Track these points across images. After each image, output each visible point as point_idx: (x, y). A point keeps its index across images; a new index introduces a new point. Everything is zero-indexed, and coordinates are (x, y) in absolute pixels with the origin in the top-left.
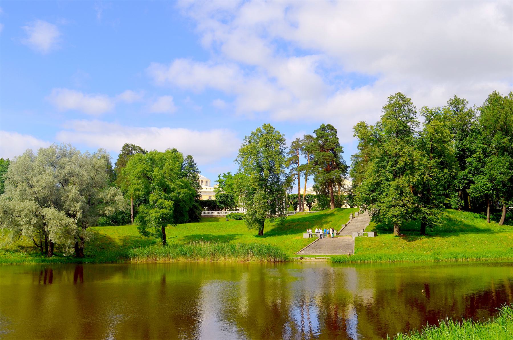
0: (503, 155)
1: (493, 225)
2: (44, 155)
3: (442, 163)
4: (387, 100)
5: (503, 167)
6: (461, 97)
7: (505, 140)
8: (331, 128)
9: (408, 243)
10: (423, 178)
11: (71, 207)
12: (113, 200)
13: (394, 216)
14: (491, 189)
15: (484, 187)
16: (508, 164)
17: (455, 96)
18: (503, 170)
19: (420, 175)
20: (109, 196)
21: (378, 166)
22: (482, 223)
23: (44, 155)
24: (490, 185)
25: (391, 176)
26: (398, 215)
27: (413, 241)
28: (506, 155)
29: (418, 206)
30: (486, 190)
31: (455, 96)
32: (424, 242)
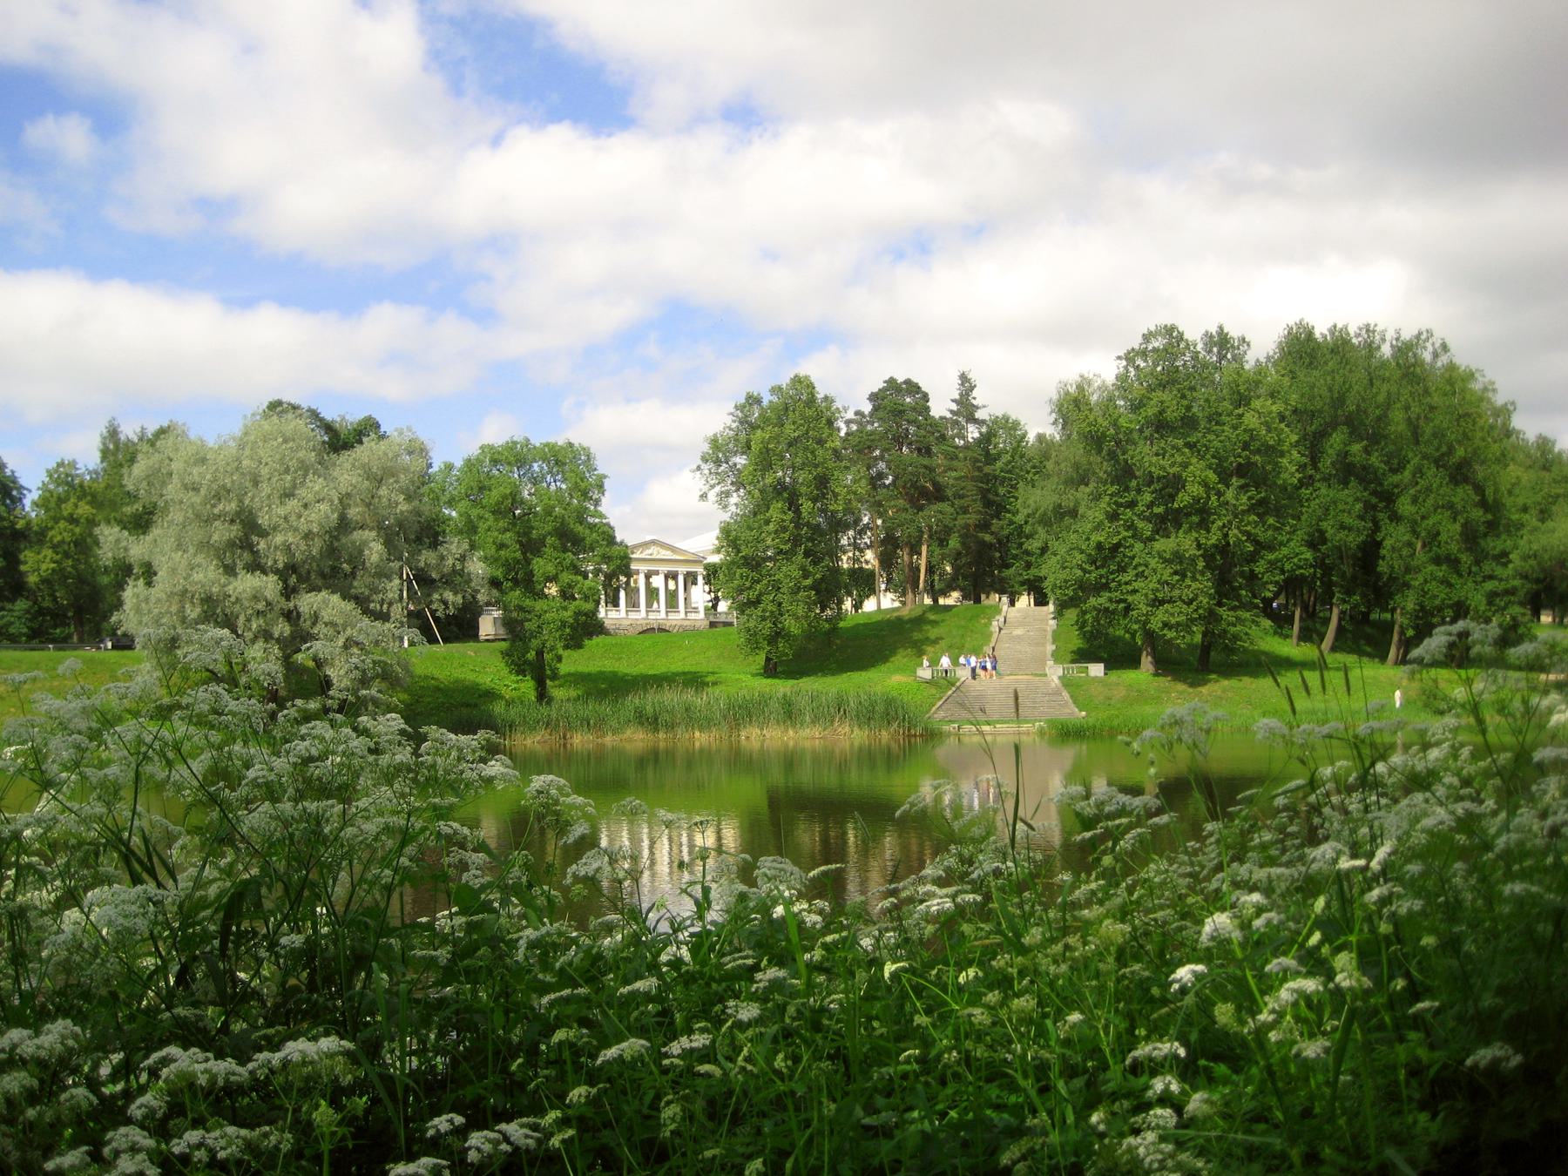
0: (1345, 483)
1: (1305, 651)
2: (285, 441)
3: (1262, 502)
4: (1140, 340)
5: (1349, 512)
6: (1234, 332)
7: (1356, 448)
8: (912, 387)
9: (1191, 690)
10: (1226, 535)
11: (375, 591)
12: (461, 573)
13: (1166, 625)
14: (1311, 566)
15: (1296, 560)
16: (1359, 506)
17: (1221, 328)
18: (1348, 521)
19: (1221, 529)
20: (450, 562)
21: (1116, 503)
22: (1290, 648)
23: (285, 441)
24: (1309, 555)
25: (1146, 528)
26: (1178, 624)
27: (1199, 685)
28: (1353, 482)
29: (278, 641)
30: (1301, 568)
31: (1221, 328)
32: (1218, 687)
